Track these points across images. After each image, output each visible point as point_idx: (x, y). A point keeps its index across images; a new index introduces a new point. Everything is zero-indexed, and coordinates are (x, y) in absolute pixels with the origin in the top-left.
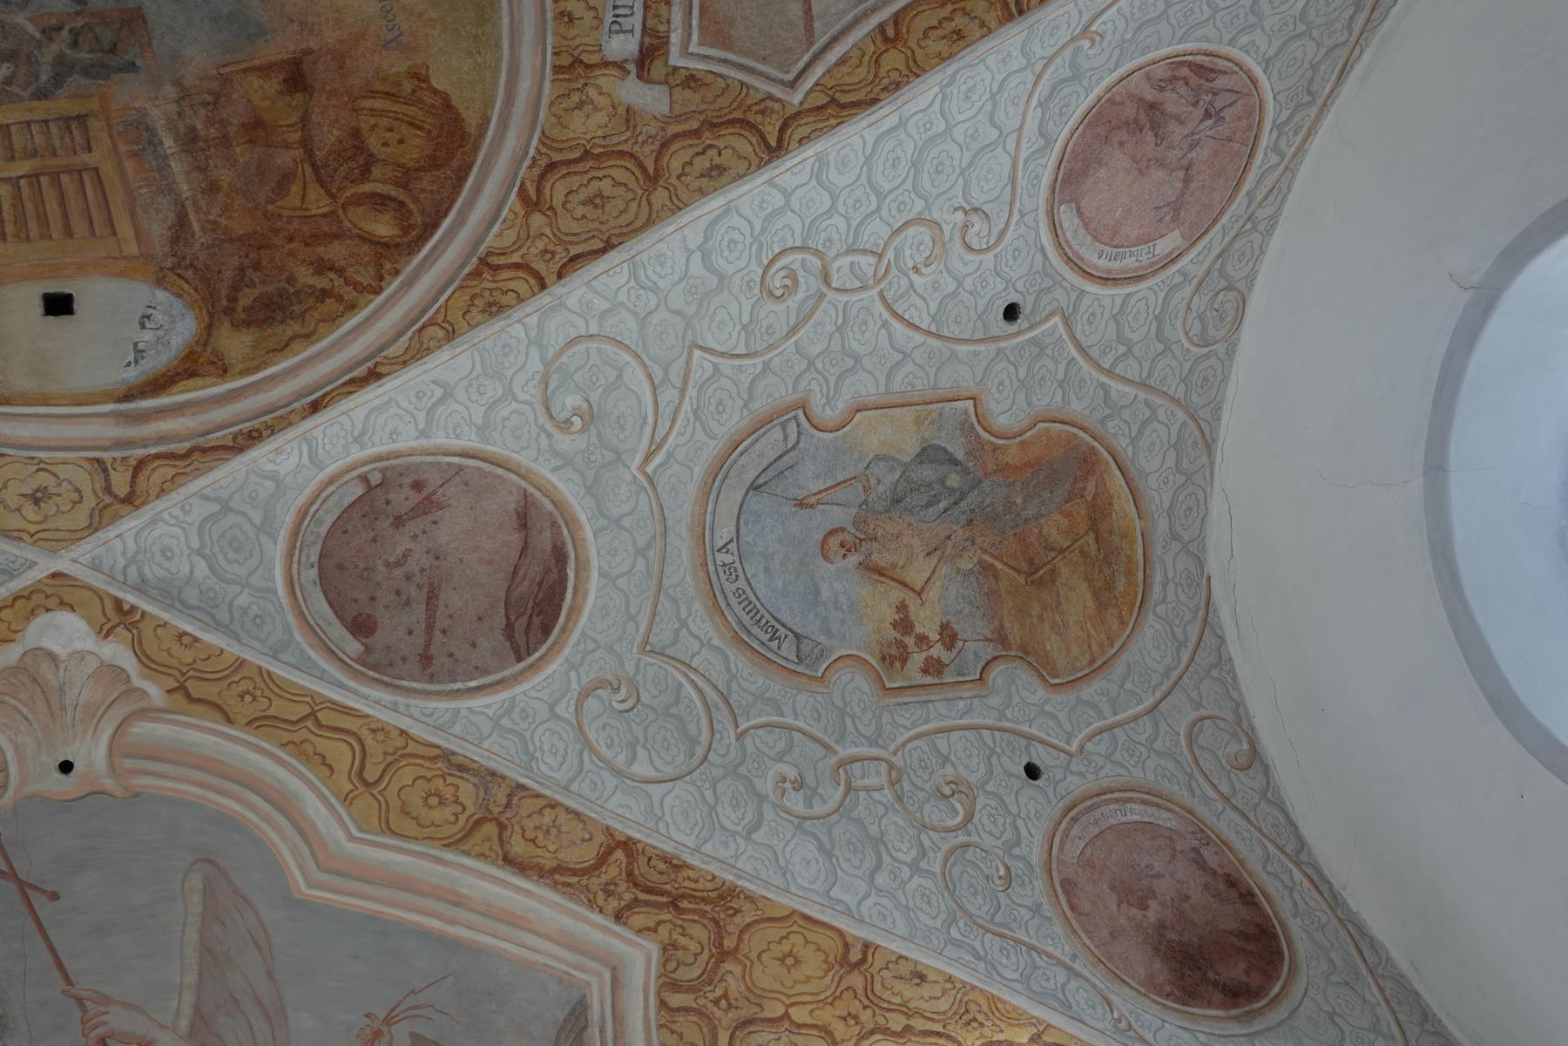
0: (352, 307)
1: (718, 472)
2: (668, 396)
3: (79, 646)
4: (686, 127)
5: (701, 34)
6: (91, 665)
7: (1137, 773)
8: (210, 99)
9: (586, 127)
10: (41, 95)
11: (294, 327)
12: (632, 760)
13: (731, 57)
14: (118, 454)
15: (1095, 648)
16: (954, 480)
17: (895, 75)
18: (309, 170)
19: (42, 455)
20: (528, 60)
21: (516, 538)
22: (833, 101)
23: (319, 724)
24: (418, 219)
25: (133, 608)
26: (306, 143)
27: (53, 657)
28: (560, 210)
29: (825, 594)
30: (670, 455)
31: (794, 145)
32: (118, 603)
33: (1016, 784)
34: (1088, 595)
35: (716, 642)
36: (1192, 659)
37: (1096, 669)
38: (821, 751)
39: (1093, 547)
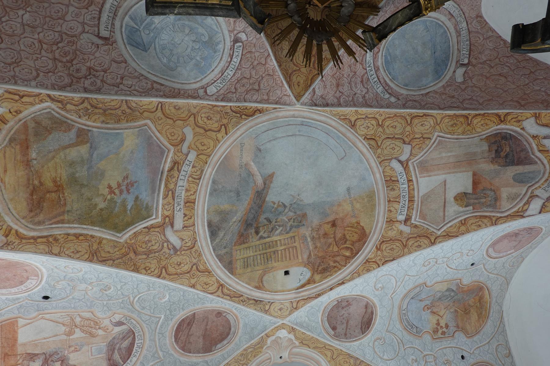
0: (340, 269)
1: (405, 296)
2: (399, 283)
3: (285, 335)
4: (414, 236)
5: (419, 217)
6: (287, 339)
7: (485, 358)
8: (317, 230)
9: (392, 234)
10: (287, 233)
11: (328, 273)
12: (384, 355)
13: (425, 222)
14: (295, 300)
15: (477, 328)
16: (452, 294)
17: (463, 232)
18: (334, 242)
19: (282, 301)
20: (381, 219)
21: (364, 310)
22: (448, 235)
23: (326, 348)
24: (355, 252)
25: (295, 328)
26: (334, 237)
27: (280, 338)
28: (384, 251)
29: (423, 318)
30: (396, 294)
31: (437, 243)
32: (292, 327)
33: (460, 361)
34: (477, 316)
35: (401, 329)
36: (497, 330)
37: (477, 333)
38: (420, 353)
39: (479, 305)
